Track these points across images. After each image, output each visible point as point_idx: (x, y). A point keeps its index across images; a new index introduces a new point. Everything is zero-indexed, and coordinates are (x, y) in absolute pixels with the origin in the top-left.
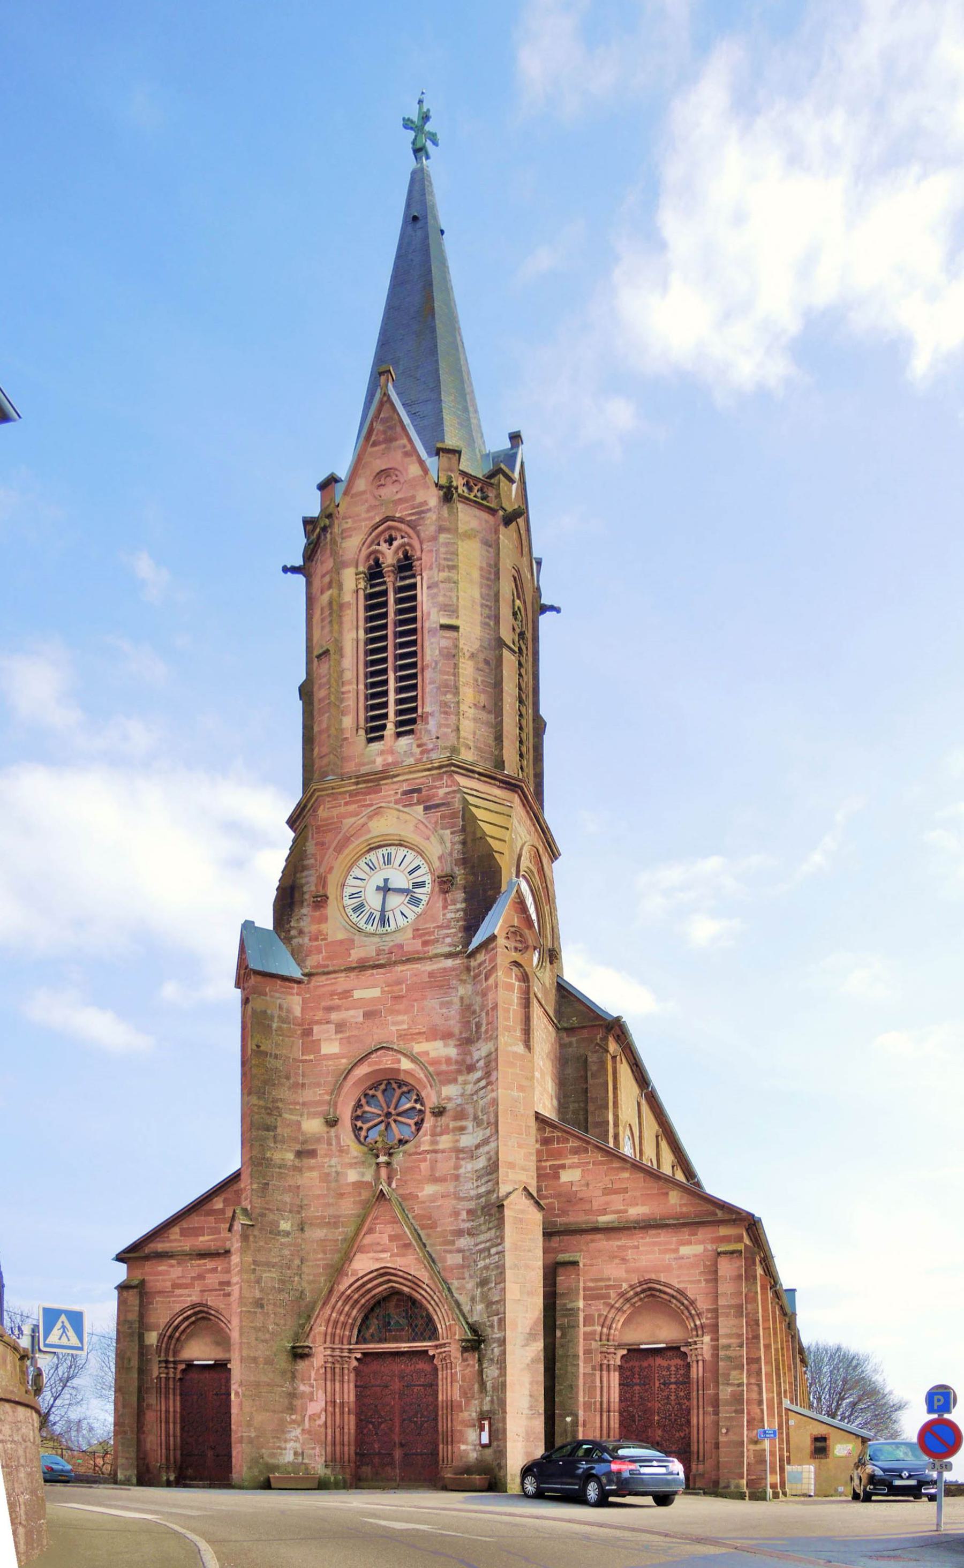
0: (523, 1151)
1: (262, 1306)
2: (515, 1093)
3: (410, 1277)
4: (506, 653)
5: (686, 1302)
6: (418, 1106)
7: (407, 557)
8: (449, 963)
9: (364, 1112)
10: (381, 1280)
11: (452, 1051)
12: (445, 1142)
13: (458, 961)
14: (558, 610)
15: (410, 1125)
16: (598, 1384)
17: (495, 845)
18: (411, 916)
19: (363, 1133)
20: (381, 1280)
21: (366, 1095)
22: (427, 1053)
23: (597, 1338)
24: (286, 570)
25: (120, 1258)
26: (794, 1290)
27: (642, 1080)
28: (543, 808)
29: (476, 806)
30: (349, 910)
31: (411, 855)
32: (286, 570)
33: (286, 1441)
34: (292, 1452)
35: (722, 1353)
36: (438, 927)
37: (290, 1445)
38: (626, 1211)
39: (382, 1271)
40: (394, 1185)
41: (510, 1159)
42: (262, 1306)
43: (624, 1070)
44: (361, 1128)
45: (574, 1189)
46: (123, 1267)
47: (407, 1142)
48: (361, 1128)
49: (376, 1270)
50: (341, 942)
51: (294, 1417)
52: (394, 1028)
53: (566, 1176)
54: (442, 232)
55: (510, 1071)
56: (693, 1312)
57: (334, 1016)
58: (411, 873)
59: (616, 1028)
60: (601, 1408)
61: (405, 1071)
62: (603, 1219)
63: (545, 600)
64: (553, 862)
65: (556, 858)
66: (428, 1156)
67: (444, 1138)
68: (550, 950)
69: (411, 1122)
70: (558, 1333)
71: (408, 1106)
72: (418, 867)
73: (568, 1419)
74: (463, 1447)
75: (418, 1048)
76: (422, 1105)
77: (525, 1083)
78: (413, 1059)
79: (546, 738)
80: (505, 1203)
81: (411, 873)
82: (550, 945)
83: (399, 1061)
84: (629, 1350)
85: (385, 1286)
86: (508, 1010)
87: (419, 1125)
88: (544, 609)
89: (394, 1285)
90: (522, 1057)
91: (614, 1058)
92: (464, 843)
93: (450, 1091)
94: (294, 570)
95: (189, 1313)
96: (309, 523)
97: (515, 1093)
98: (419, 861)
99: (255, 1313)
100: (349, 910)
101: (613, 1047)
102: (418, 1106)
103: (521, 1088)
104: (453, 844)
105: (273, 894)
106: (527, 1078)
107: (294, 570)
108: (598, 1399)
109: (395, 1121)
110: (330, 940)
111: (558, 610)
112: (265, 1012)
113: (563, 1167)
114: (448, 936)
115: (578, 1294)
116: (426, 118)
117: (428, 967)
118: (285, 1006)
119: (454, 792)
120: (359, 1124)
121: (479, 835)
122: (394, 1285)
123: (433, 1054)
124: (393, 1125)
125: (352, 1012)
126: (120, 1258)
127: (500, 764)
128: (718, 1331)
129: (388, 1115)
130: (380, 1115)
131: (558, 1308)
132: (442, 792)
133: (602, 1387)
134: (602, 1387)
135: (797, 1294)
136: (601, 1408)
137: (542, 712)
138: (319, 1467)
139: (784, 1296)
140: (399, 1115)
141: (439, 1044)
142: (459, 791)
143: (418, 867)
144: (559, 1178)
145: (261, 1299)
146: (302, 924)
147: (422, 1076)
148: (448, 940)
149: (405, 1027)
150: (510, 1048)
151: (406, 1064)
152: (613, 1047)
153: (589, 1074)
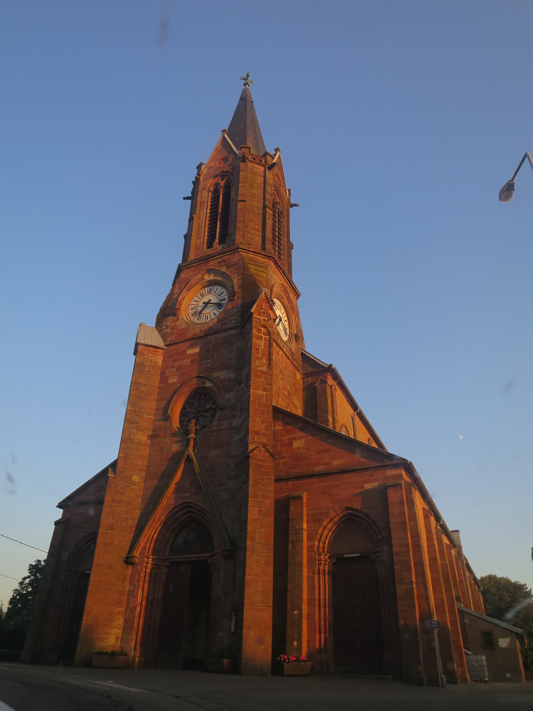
0: (264, 425)
1: (112, 529)
2: (261, 392)
3: (199, 508)
4: (268, 210)
5: (370, 522)
6: (214, 406)
7: (228, 183)
8: (233, 332)
9: (187, 412)
10: (184, 511)
11: (232, 375)
12: (225, 424)
13: (237, 331)
14: (298, 206)
15: (208, 417)
16: (317, 585)
17: (256, 277)
18: (218, 313)
19: (185, 423)
20: (184, 511)
21: (188, 403)
22: (219, 377)
23: (316, 550)
24: (184, 198)
25: (60, 506)
26: (458, 531)
27: (354, 406)
28: (291, 276)
29: (250, 264)
30: (190, 315)
31: (220, 288)
32: (184, 198)
33: (111, 628)
34: (114, 637)
35: (395, 558)
36: (229, 316)
37: (114, 631)
38: (331, 463)
39: (184, 505)
40: (196, 451)
41: (256, 429)
42: (112, 529)
43: (339, 395)
44: (184, 421)
45: (301, 451)
46: (61, 511)
47: (206, 426)
48: (184, 421)
49: (181, 504)
50: (185, 328)
51: (120, 609)
52: (204, 366)
53: (296, 444)
54: (253, 102)
55: (258, 379)
56: (376, 529)
57: (176, 364)
58: (219, 296)
59: (330, 370)
60: (320, 604)
61: (207, 387)
62: (318, 469)
63: (292, 202)
64: (297, 299)
65: (299, 297)
66: (215, 433)
67: (225, 422)
68: (295, 335)
69: (209, 415)
70: (290, 546)
71: (209, 407)
72: (223, 292)
73: (296, 612)
74: (221, 634)
75: (215, 375)
76: (216, 405)
77: (267, 386)
78: (211, 381)
79: (293, 252)
80: (250, 455)
81: (219, 296)
82: (295, 333)
83: (205, 383)
84: (337, 559)
85: (187, 516)
86: (258, 349)
87: (213, 416)
88: (292, 206)
89: (192, 514)
90: (265, 373)
91: (331, 386)
92: (243, 279)
93: (230, 396)
94: (188, 198)
95: (88, 539)
96: (193, 182)
97: (261, 392)
98: (223, 290)
99: (107, 533)
100: (190, 315)
101: (330, 381)
102: (214, 406)
103: (264, 389)
104: (238, 280)
105: (158, 311)
106: (268, 384)
107: (188, 198)
108: (317, 597)
109: (202, 416)
110: (179, 328)
111: (298, 206)
112: (143, 363)
113: (294, 439)
114: (233, 320)
115: (302, 518)
116: (248, 76)
117: (224, 335)
118: (154, 360)
119: (240, 259)
120: (183, 418)
121: (249, 275)
122: (192, 514)
123: (222, 377)
124: (200, 417)
125: (185, 361)
126: (60, 506)
127: (264, 248)
128: (391, 542)
129: (199, 412)
130: (193, 413)
131: (290, 528)
132: (234, 260)
133: (319, 587)
134: (319, 587)
135: (460, 533)
136: (320, 604)
137: (291, 240)
138: (134, 652)
139: (453, 535)
140: (204, 412)
141: (225, 372)
142: (242, 258)
143: (223, 292)
144: (292, 445)
145: (112, 524)
146: (168, 323)
147: (216, 389)
148: (233, 322)
149: (209, 365)
150: (258, 368)
151: (208, 384)
152: (330, 381)
153: (317, 395)
